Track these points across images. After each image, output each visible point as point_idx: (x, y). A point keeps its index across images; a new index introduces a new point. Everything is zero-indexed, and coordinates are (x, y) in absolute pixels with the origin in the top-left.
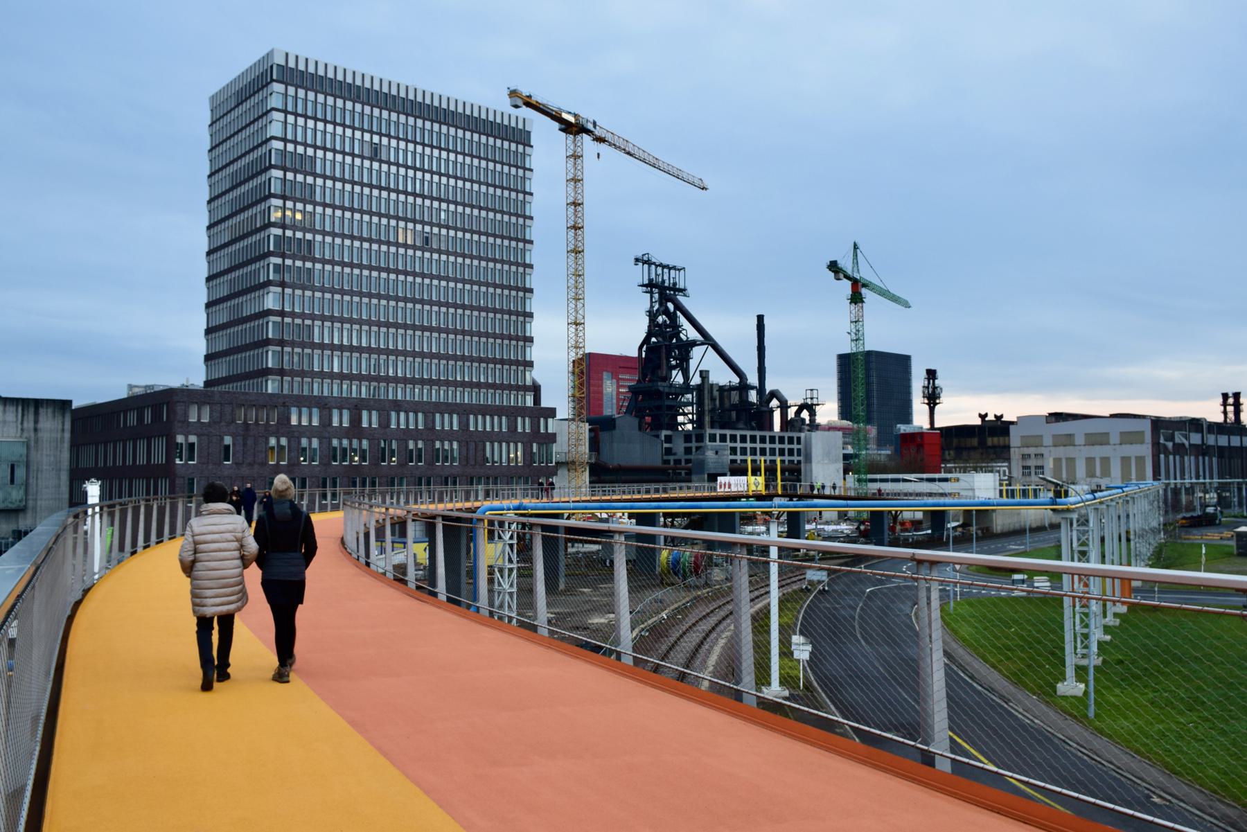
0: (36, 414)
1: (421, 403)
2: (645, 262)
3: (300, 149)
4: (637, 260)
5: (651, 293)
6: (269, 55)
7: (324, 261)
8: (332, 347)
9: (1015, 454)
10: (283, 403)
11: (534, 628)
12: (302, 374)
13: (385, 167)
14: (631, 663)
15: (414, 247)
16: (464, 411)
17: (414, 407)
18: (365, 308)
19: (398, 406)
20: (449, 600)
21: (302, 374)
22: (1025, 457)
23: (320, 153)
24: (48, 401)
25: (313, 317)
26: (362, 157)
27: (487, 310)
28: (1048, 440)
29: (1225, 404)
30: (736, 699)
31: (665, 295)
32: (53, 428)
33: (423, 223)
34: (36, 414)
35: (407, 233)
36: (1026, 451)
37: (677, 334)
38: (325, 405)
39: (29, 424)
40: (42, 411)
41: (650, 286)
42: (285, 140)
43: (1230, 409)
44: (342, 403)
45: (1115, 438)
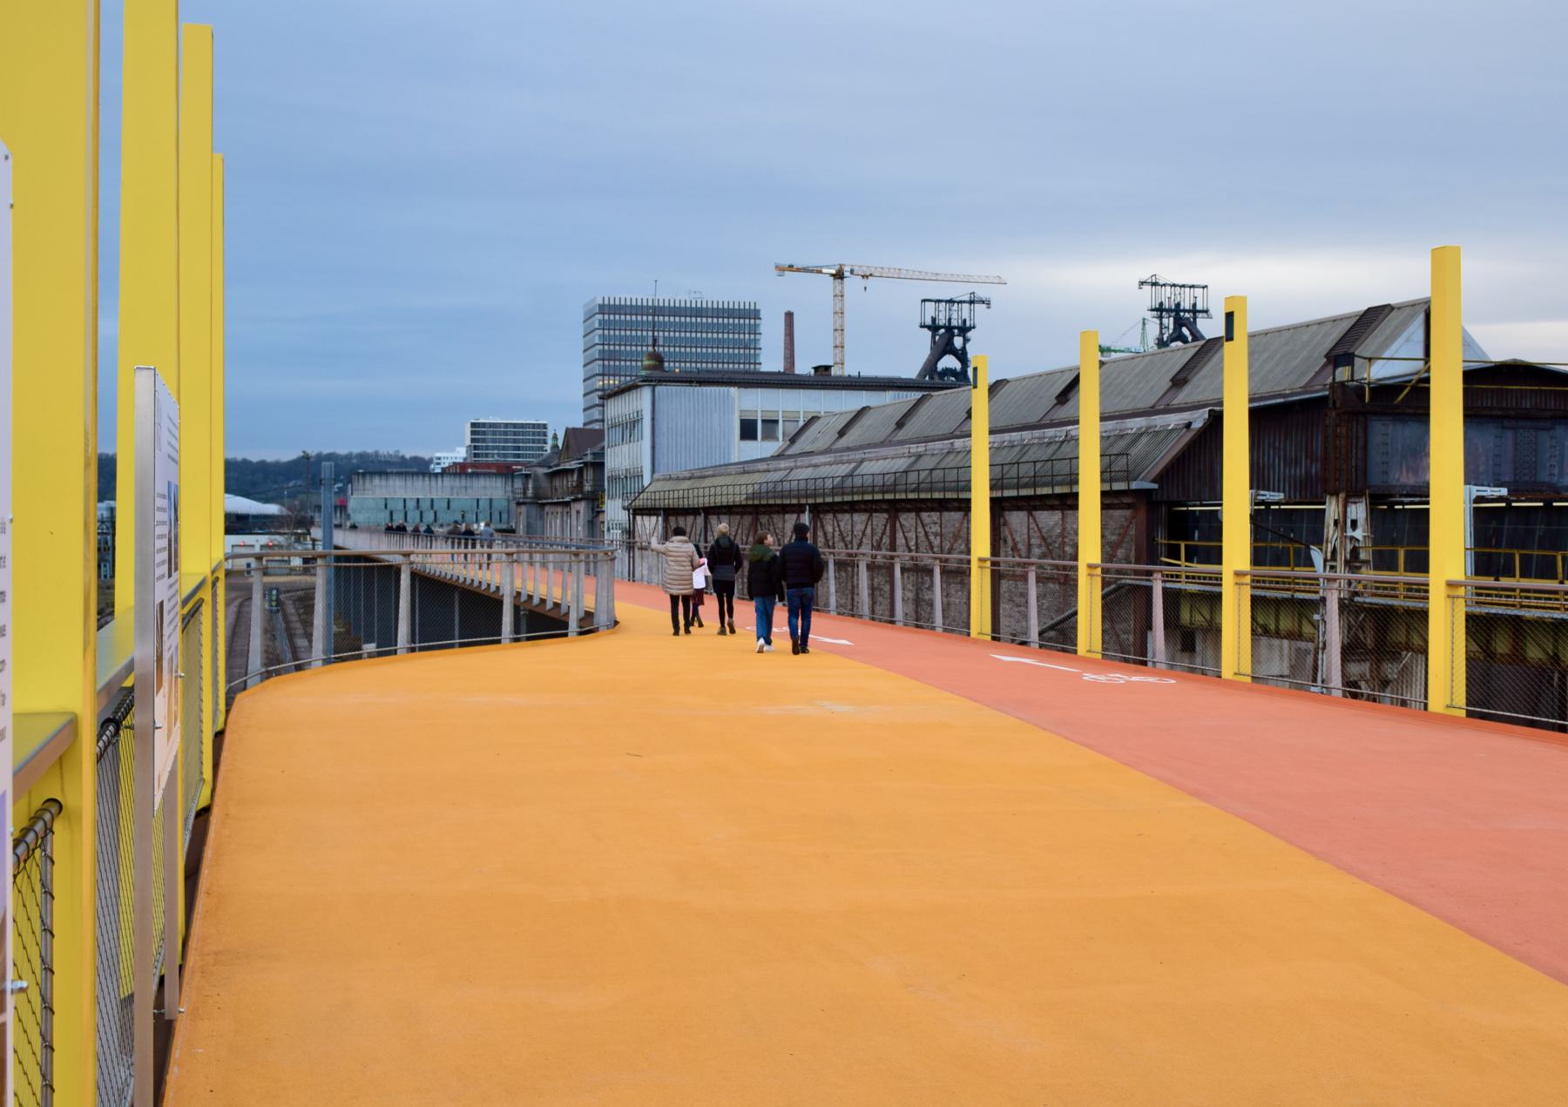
5: (1161, 318)
41: (1160, 310)
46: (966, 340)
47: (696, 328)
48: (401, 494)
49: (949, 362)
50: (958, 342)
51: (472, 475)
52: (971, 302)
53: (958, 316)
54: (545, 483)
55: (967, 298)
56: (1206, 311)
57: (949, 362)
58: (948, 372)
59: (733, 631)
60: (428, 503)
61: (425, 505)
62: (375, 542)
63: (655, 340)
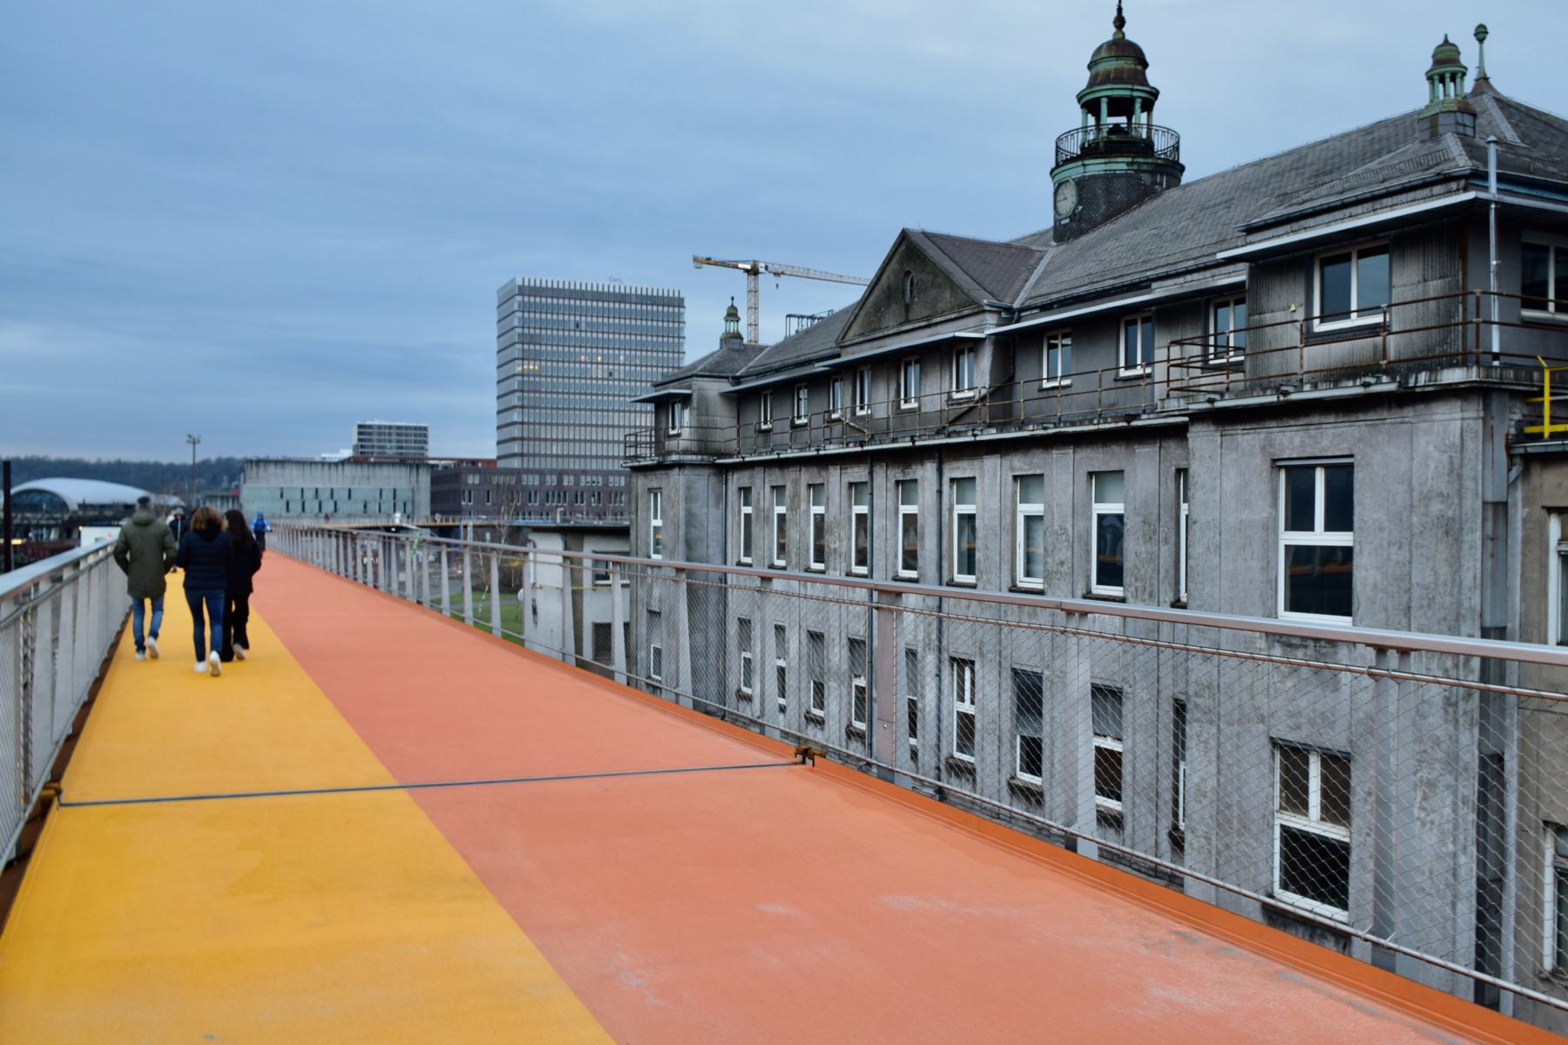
6: (513, 280)
10: (518, 473)
11: (463, 620)
14: (1095, 855)
17: (596, 473)
19: (585, 472)
20: (506, 637)
30: (1067, 848)
32: (425, 478)
35: (600, 371)
44: (551, 472)
47: (620, 315)
48: (298, 484)
51: (374, 464)
54: (723, 417)
60: (328, 493)
61: (324, 495)
62: (1466, 935)
63: (577, 325)
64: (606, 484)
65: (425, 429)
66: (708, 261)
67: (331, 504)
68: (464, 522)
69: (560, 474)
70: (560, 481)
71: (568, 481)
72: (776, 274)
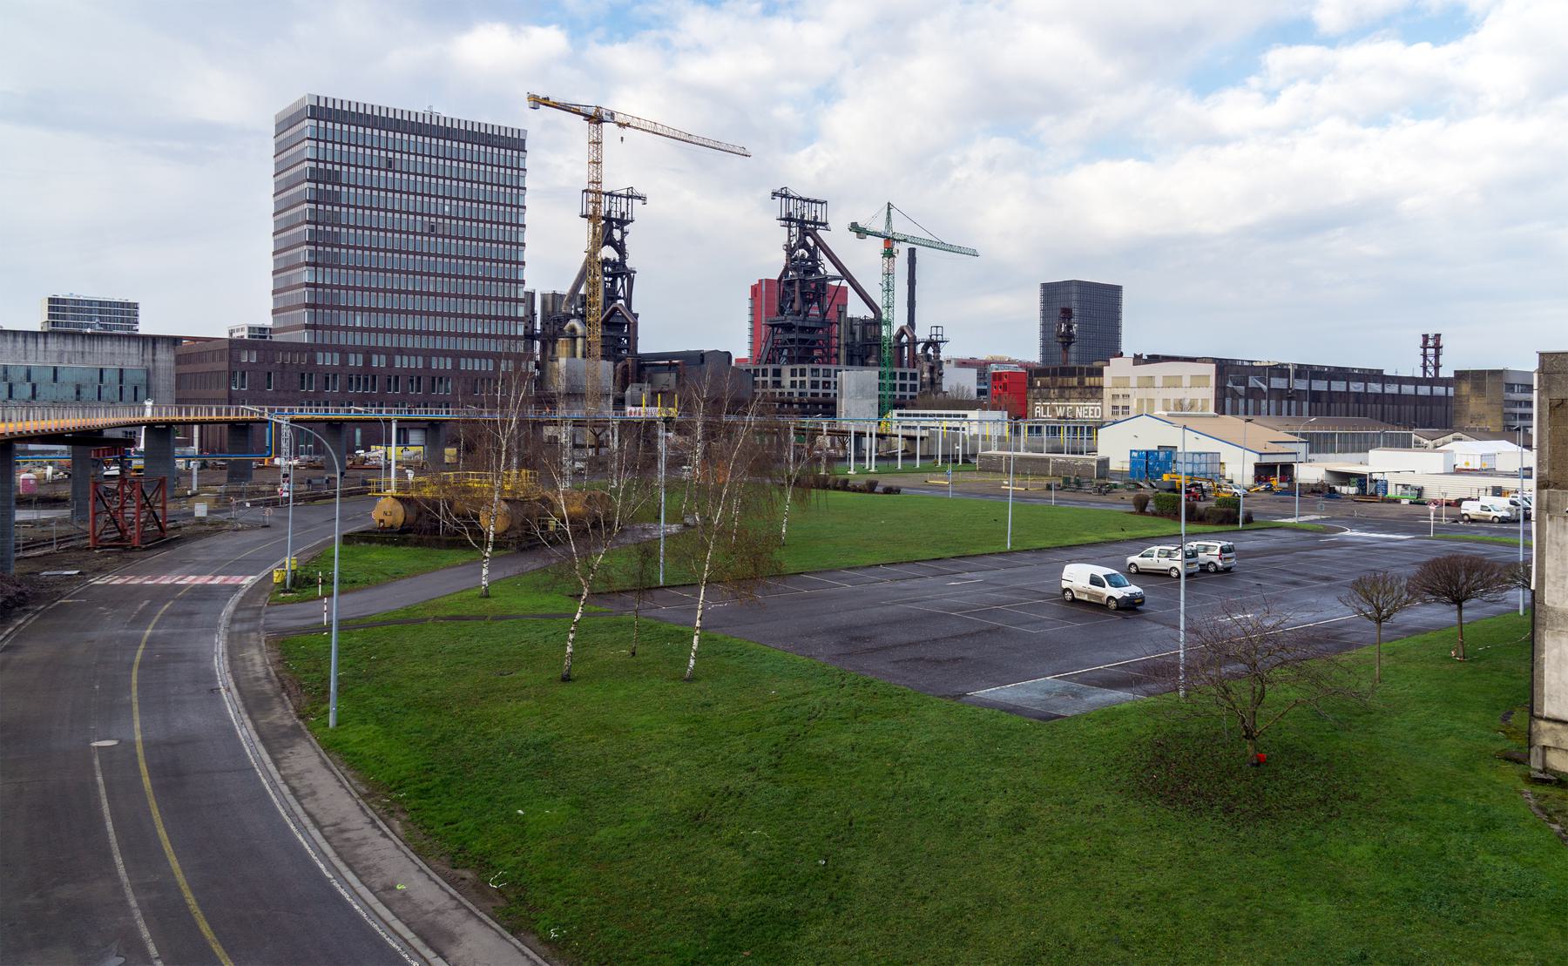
0: (154, 348)
1: (420, 350)
2: (783, 196)
3: (329, 167)
4: (775, 194)
7: (348, 247)
8: (355, 309)
9: (1107, 393)
12: (331, 328)
13: (398, 175)
15: (422, 234)
16: (457, 355)
17: (415, 352)
18: (381, 281)
19: (400, 351)
21: (331, 328)
22: (1115, 397)
23: (345, 169)
24: (163, 338)
25: (339, 287)
26: (379, 169)
27: (484, 279)
28: (1133, 382)
29: (1425, 347)
31: (805, 229)
32: (165, 357)
33: (430, 215)
34: (154, 348)
36: (1116, 391)
37: (815, 269)
38: (344, 351)
39: (148, 356)
40: (158, 346)
41: (788, 219)
42: (317, 161)
43: (1431, 351)
44: (356, 350)
45: (1186, 381)
46: (624, 234)
49: (608, 252)
50: (617, 234)
52: (628, 197)
53: (618, 208)
55: (624, 192)
56: (825, 224)
57: (608, 252)
58: (606, 262)
59: (1426, 337)
60: (23, 373)
64: (428, 366)
65: (135, 306)
66: (546, 102)
67: (28, 387)
68: (384, 415)
69: (368, 352)
70: (367, 362)
71: (378, 362)
72: (620, 125)
